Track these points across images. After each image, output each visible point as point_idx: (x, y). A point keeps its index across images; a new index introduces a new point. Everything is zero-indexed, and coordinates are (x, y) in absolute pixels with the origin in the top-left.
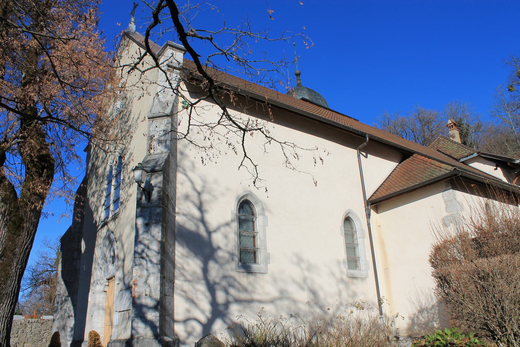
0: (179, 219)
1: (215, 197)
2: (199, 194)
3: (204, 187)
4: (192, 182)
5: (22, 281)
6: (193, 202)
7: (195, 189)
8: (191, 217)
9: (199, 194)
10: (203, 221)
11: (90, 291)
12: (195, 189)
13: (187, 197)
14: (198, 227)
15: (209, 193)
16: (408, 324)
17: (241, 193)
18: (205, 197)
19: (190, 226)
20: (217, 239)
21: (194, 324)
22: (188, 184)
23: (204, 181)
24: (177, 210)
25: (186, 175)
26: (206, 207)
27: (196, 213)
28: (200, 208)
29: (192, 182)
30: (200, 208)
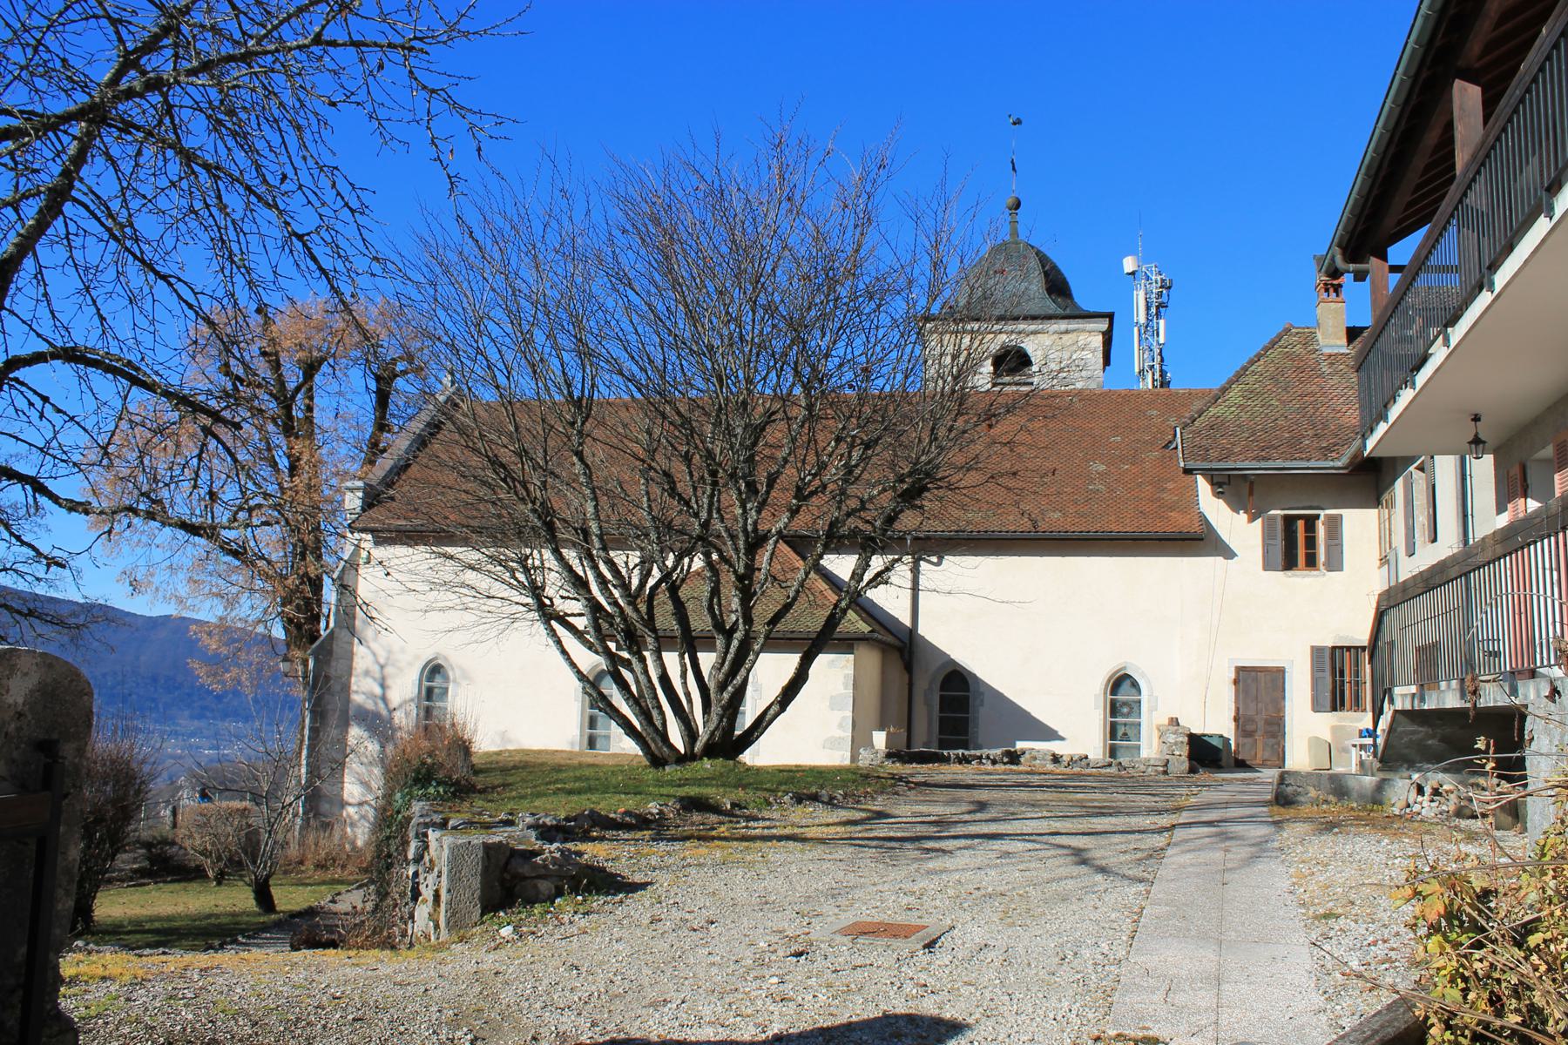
0: (357, 698)
1: (401, 670)
2: (382, 667)
3: (388, 658)
4: (374, 654)
5: (871, 1016)
6: (375, 679)
7: (378, 662)
8: (372, 696)
9: (382, 667)
10: (384, 698)
11: (675, 1037)
12: (378, 662)
13: (367, 673)
14: (376, 704)
15: (393, 665)
16: (941, 558)
17: (427, 655)
18: (389, 670)
19: (370, 705)
20: (399, 718)
21: (367, 807)
22: (371, 657)
23: (390, 652)
24: (354, 687)
25: (369, 647)
26: (389, 682)
27: (378, 691)
28: (383, 686)
29: (374, 654)
30: (383, 686)
